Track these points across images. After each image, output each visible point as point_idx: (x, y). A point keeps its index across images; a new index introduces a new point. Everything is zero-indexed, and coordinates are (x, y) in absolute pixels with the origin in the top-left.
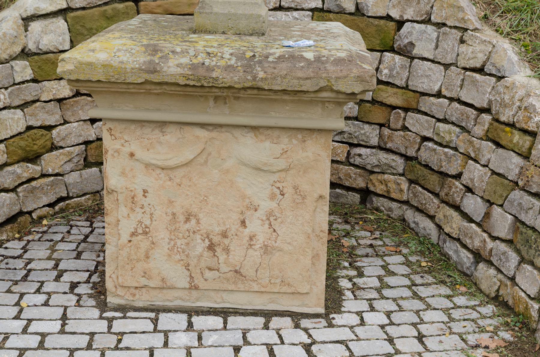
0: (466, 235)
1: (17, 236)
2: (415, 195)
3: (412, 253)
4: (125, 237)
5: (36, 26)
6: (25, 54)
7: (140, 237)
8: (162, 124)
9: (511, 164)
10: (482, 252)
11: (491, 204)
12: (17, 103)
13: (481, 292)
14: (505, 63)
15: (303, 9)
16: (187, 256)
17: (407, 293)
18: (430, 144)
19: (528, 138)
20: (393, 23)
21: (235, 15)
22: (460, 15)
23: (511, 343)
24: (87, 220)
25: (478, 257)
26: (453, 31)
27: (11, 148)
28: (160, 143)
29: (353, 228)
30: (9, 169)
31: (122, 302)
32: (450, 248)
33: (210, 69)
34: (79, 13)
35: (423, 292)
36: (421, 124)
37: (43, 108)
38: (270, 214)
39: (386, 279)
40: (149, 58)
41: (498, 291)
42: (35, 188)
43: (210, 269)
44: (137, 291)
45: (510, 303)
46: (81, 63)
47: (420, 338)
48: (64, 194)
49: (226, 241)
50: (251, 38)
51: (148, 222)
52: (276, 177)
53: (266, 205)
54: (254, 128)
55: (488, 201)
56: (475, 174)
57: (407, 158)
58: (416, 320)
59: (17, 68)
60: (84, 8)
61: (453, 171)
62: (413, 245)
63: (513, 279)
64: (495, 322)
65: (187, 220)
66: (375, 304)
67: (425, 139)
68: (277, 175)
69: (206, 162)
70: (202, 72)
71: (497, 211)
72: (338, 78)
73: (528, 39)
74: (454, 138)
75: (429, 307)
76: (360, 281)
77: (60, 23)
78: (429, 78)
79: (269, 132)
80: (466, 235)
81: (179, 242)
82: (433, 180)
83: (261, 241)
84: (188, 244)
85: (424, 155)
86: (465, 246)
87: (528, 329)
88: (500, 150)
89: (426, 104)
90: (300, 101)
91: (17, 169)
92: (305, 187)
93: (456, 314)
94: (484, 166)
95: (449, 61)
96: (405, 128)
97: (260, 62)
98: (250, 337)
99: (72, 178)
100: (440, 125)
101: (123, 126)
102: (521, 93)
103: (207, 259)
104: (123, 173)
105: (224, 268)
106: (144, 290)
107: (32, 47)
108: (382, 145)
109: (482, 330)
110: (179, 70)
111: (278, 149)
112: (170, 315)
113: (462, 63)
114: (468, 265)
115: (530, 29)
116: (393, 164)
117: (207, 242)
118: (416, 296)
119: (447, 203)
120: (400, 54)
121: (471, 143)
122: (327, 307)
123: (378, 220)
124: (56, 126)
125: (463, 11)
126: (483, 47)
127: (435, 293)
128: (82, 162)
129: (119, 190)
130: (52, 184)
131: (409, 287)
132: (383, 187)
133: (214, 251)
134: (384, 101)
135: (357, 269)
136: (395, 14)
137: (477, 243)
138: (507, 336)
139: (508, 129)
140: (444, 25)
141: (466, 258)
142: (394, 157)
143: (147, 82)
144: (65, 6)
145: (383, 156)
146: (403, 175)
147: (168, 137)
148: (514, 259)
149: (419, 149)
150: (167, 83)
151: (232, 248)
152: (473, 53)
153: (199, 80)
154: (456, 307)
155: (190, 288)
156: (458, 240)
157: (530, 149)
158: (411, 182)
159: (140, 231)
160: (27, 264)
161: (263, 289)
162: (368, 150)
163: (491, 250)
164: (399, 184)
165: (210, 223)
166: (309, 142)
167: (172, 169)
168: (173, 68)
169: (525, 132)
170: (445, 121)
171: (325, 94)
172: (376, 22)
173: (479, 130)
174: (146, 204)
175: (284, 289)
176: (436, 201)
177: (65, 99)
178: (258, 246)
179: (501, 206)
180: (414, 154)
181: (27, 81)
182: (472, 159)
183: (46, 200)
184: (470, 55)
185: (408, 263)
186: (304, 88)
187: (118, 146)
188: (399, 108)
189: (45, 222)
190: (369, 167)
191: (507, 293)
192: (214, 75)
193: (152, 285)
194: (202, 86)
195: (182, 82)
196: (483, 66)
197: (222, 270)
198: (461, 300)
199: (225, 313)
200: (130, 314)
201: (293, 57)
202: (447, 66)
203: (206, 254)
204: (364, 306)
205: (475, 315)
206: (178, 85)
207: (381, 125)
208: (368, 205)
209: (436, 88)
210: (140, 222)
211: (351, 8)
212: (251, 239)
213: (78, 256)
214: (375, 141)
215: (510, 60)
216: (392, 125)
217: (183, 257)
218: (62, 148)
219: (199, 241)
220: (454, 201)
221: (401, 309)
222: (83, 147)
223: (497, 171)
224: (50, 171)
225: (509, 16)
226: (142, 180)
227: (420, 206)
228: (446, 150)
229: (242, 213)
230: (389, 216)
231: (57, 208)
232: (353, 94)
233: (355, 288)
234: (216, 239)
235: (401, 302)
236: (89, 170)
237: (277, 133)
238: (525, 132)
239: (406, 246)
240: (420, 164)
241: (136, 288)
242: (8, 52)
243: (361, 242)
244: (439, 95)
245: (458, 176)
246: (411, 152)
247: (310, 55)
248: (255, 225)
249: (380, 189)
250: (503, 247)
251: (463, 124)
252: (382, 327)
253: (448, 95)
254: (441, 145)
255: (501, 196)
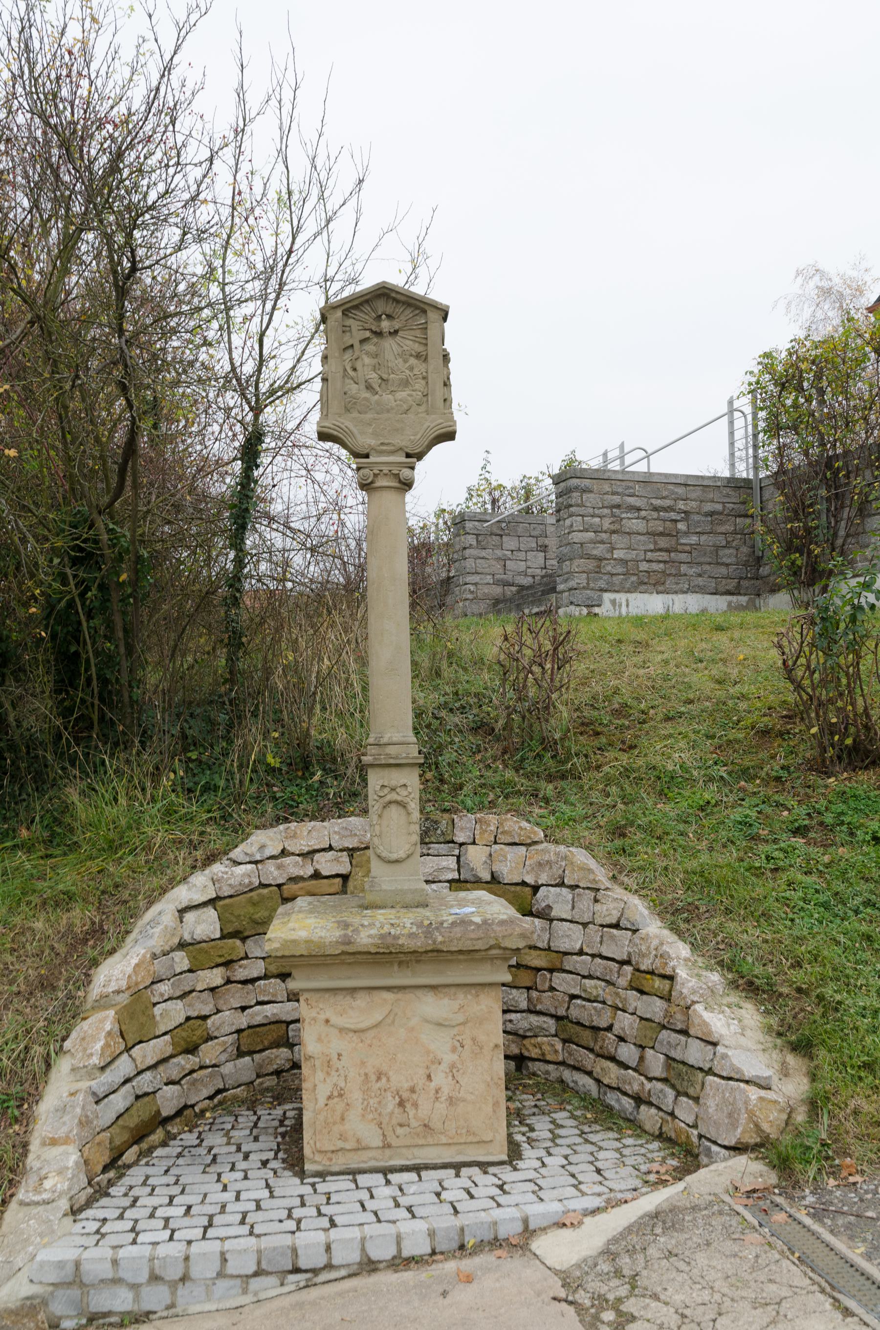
0: (624, 1082)
1: (186, 1129)
2: (570, 1054)
3: (577, 1109)
4: (322, 1101)
5: (189, 917)
6: (182, 945)
7: (336, 1100)
8: (353, 991)
9: (655, 1008)
10: (641, 1095)
11: (642, 1047)
12: (178, 993)
13: (646, 1132)
14: (638, 917)
15: (440, 881)
16: (380, 1114)
17: (579, 1140)
18: (579, 1001)
19: (667, 982)
20: (528, 889)
21: (401, 890)
22: (591, 877)
23: (678, 1167)
24: (248, 1109)
25: (639, 1100)
26: (587, 891)
27: (176, 1040)
28: (352, 1008)
29: (514, 1092)
30: (175, 1060)
31: (319, 1168)
32: (611, 1098)
33: (396, 937)
34: (227, 901)
35: (592, 1137)
36: (568, 983)
37: (199, 998)
38: (453, 1066)
39: (556, 1131)
40: (343, 932)
41: (661, 1128)
42: (196, 1080)
43: (401, 1125)
44: (333, 1156)
45: (673, 1136)
46: (286, 941)
47: (598, 1171)
48: (221, 1087)
49: (415, 1096)
50: (418, 910)
51: (342, 1085)
52: (455, 1031)
53: (449, 1058)
54: (433, 988)
55: (641, 1046)
56: (625, 1023)
57: (558, 1018)
58: (591, 1159)
59: (177, 959)
60: (231, 896)
61: (604, 1024)
62: (576, 1102)
63: (672, 1114)
64: (662, 1154)
65: (379, 1079)
66: (552, 1151)
67: (573, 997)
68: (456, 1029)
69: (393, 1022)
70: (389, 940)
71: (649, 1052)
72: (504, 937)
73: (654, 894)
74: (601, 992)
75: (601, 1148)
76: (533, 1135)
77: (211, 913)
78: (570, 938)
79: (447, 990)
80: (624, 1082)
81: (372, 1101)
82: (586, 1036)
83: (446, 1093)
84: (380, 1102)
85: (574, 1013)
86: (625, 1094)
87: (692, 1155)
88: (645, 997)
89: (570, 963)
90: (473, 960)
91: (180, 1060)
92: (482, 1038)
93: (626, 1152)
94: (632, 1014)
95: (586, 920)
96: (552, 989)
97: (437, 928)
98: (445, 1184)
99: (227, 1069)
100: (586, 981)
101: (318, 995)
102: (655, 943)
103: (398, 1116)
104: (319, 1040)
105: (414, 1123)
106: (340, 1153)
107: (187, 937)
108: (532, 1008)
109: (652, 1161)
110: (370, 941)
111: (455, 1005)
112: (366, 1176)
113: (598, 921)
114: (630, 1110)
115: (655, 886)
116: (545, 1026)
117: (397, 1099)
118: (587, 1141)
119: (603, 1057)
120: (538, 917)
121: (617, 994)
122: (509, 1156)
123: (537, 1084)
124: (210, 1016)
125: (593, 873)
126: (616, 905)
127: (604, 1138)
128: (235, 1052)
129: (316, 1056)
130: (211, 1076)
131: (580, 1136)
132: (537, 1050)
133: (404, 1107)
134: (529, 964)
135: (527, 1125)
136: (530, 880)
137: (636, 1087)
138: (675, 1163)
139: (648, 976)
140: (577, 886)
141: (628, 1104)
142: (545, 1019)
143: (343, 953)
144: (214, 896)
145: (534, 1020)
146: (556, 1036)
147: (358, 1002)
148: (670, 1093)
149: (568, 1008)
150: (360, 953)
151: (420, 1103)
152: (608, 911)
153: (388, 948)
154: (625, 1146)
155: (384, 1147)
156: (618, 1089)
157: (670, 991)
158: (565, 1041)
159: (335, 1094)
160: (209, 1151)
161: (450, 1141)
162: (519, 1015)
163: (649, 1091)
164: (553, 1046)
165: (399, 1080)
166: (482, 997)
167: (363, 1031)
168: (365, 939)
169: (664, 977)
170: (590, 977)
171: (494, 952)
172: (513, 888)
173: (623, 982)
174: (340, 1067)
175: (471, 1139)
176: (591, 1056)
177: (217, 987)
178: (443, 1099)
179: (653, 1048)
180: (564, 1013)
181: (185, 972)
182: (620, 1009)
183: (206, 1093)
184: (605, 913)
185: (574, 1117)
186: (476, 948)
187: (314, 1014)
188: (545, 969)
189: (208, 1115)
190: (521, 1032)
191: (669, 1130)
192: (400, 942)
193: (348, 1147)
194: (391, 953)
195: (373, 950)
196: (619, 922)
197: (412, 1126)
198: (629, 1141)
199: (417, 1169)
200: (328, 1178)
201: (464, 922)
202: (585, 925)
203: (397, 1110)
204: (542, 1153)
205: (643, 1151)
206: (370, 953)
207: (528, 989)
208: (524, 1072)
209: (578, 947)
210: (335, 1085)
211: (487, 877)
212: (437, 1092)
213: (256, 1139)
214: (524, 1005)
215: (641, 914)
216: (539, 987)
217: (377, 1116)
218: (216, 1038)
219: (390, 1098)
220: (609, 1053)
221: (575, 1152)
222: (235, 1035)
223: (644, 1016)
224: (208, 1062)
225: (635, 874)
226: (337, 1044)
227: (576, 1064)
228: (595, 1004)
229: (427, 1067)
230: (546, 1079)
231: (216, 1101)
232: (518, 949)
233: (530, 1141)
234: (405, 1095)
235: (575, 1147)
236: (242, 1060)
237: (453, 990)
238: (664, 977)
239: (569, 1103)
240: (571, 1022)
241: (333, 1152)
242: (170, 943)
243: (525, 1104)
244: (581, 953)
245: (609, 1028)
246: (561, 1012)
247: (477, 919)
248: (441, 1079)
249: (535, 1053)
250: (659, 1085)
251: (608, 978)
252: (563, 1167)
253: (590, 952)
254: (589, 1000)
255: (651, 1039)
